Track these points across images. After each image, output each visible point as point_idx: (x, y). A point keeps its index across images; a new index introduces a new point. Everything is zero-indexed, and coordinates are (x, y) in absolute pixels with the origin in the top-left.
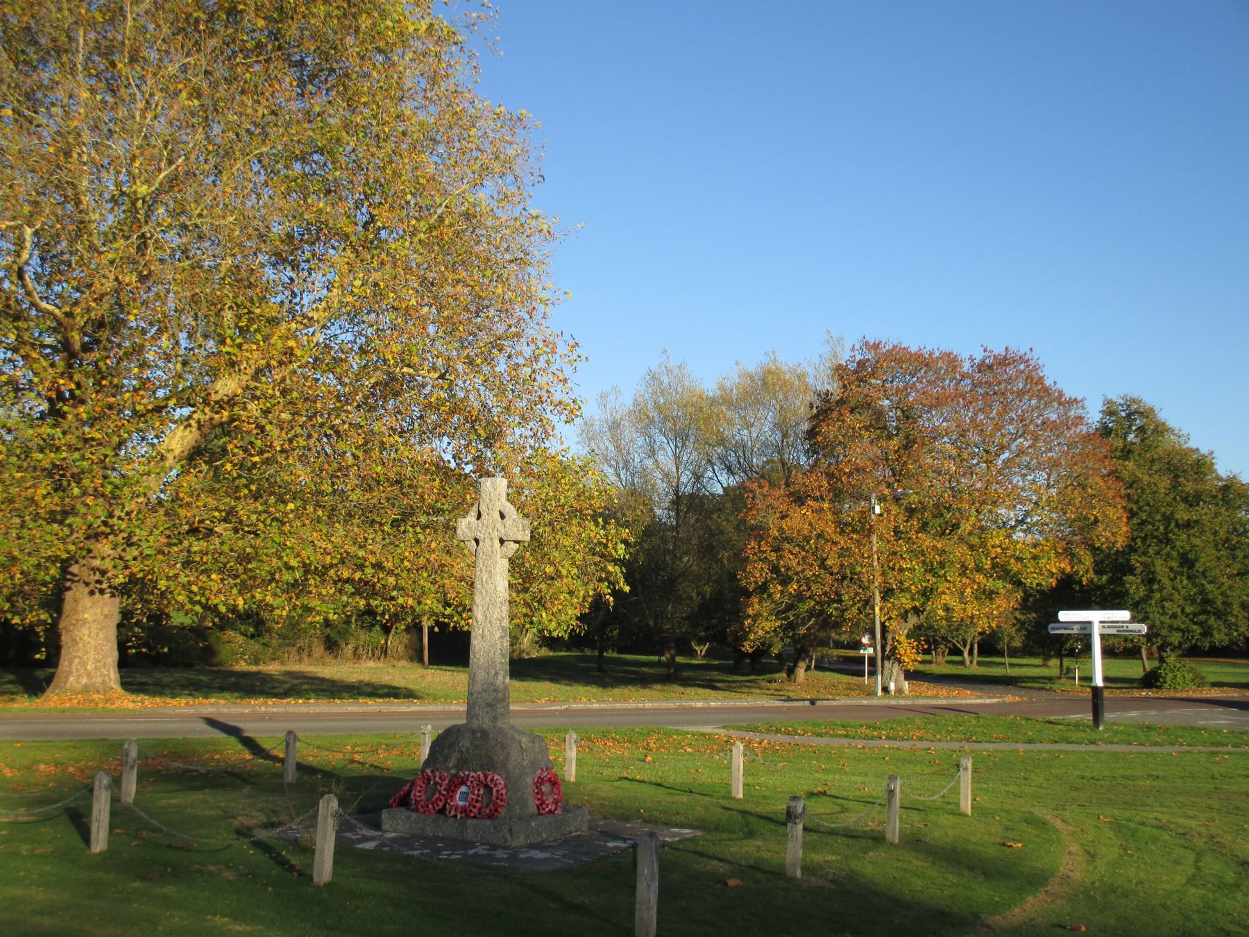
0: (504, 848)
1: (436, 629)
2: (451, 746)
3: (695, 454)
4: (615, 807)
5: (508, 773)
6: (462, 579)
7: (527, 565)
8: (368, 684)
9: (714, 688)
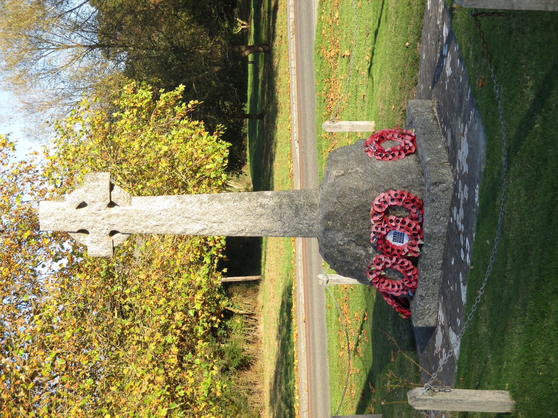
0: (456, 190)
1: (225, 270)
2: (342, 253)
3: (54, 30)
4: (403, 74)
5: (372, 189)
6: (175, 249)
7: (160, 185)
8: (280, 331)
9: (276, 8)
